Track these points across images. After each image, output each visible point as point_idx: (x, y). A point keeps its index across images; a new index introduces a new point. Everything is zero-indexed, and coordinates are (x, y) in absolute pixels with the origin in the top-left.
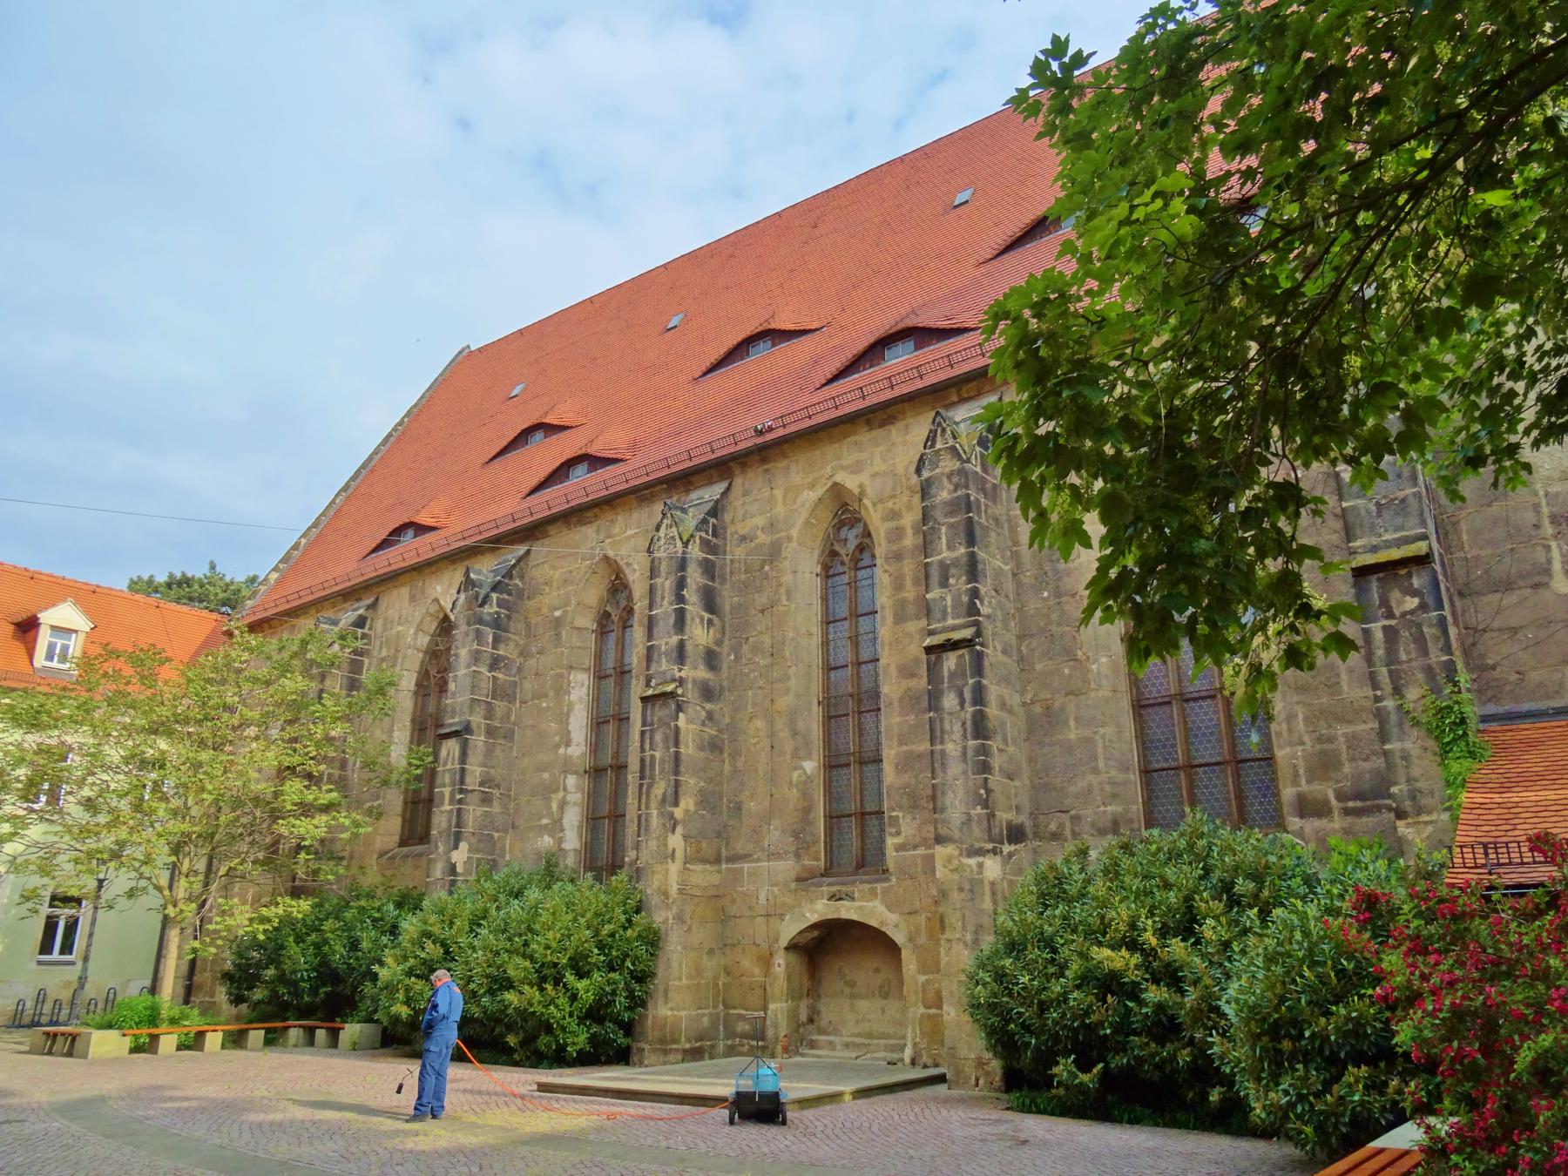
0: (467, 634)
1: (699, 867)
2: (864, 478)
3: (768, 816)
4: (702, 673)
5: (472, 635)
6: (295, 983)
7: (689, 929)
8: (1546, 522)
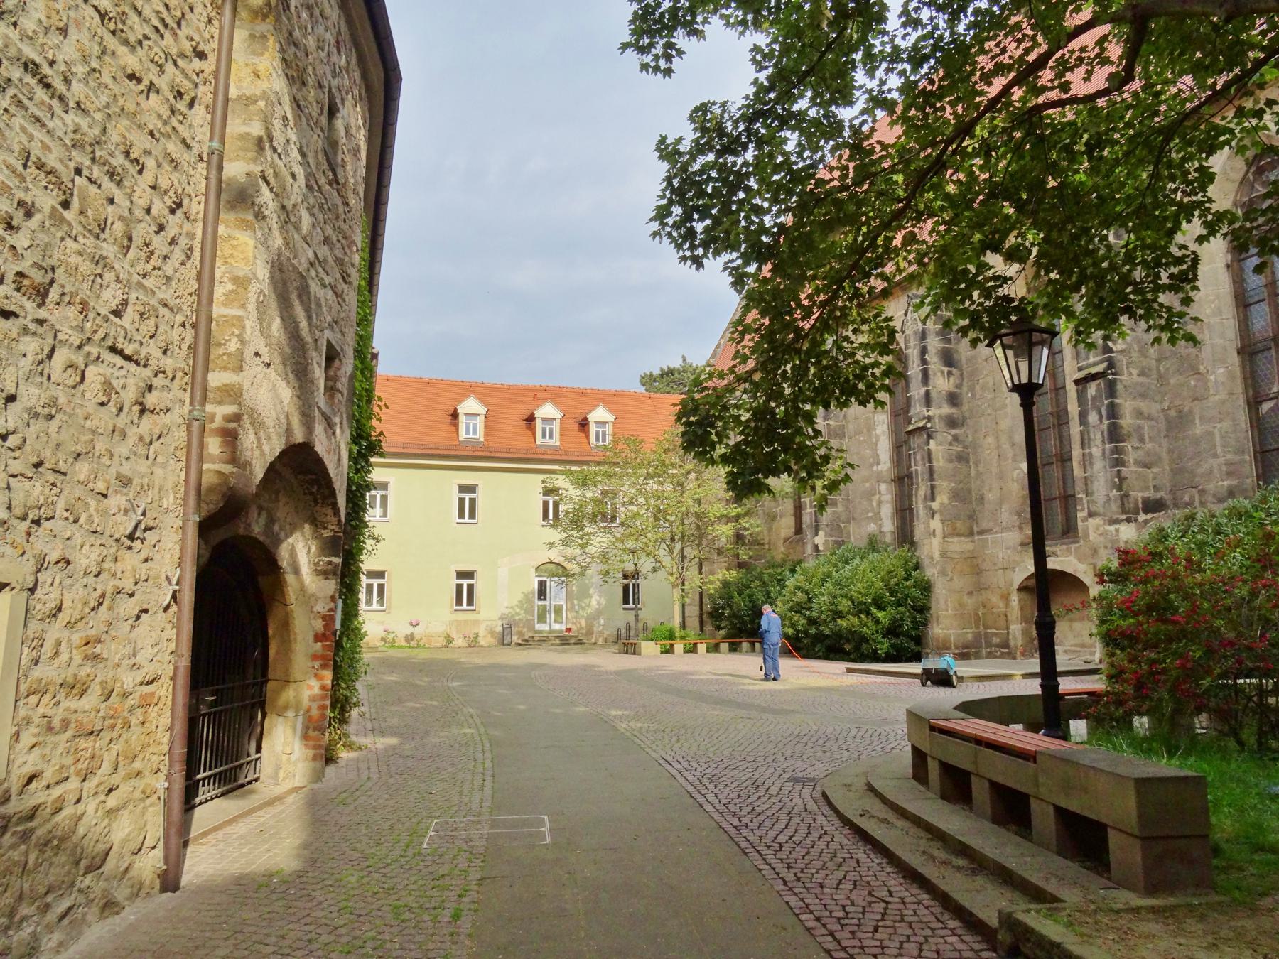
1: (956, 540)
3: (1001, 502)
4: (946, 410)
6: (741, 617)
7: (951, 579)
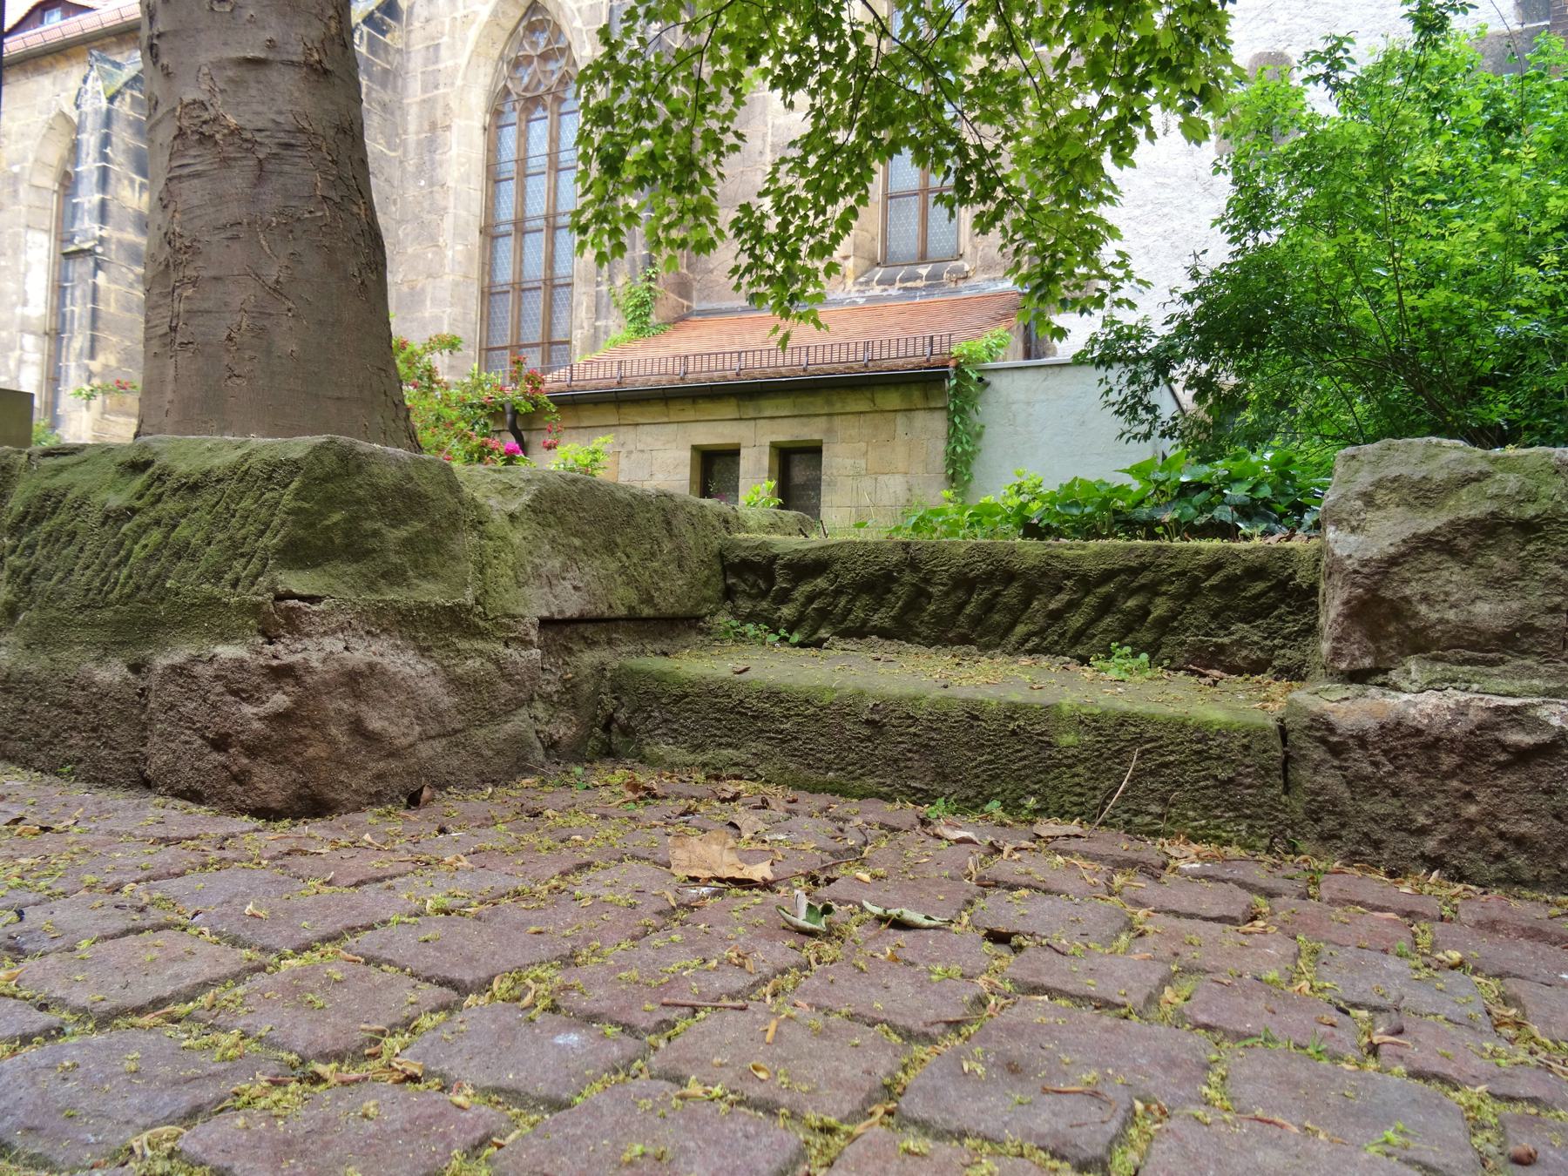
8: (768, 150)
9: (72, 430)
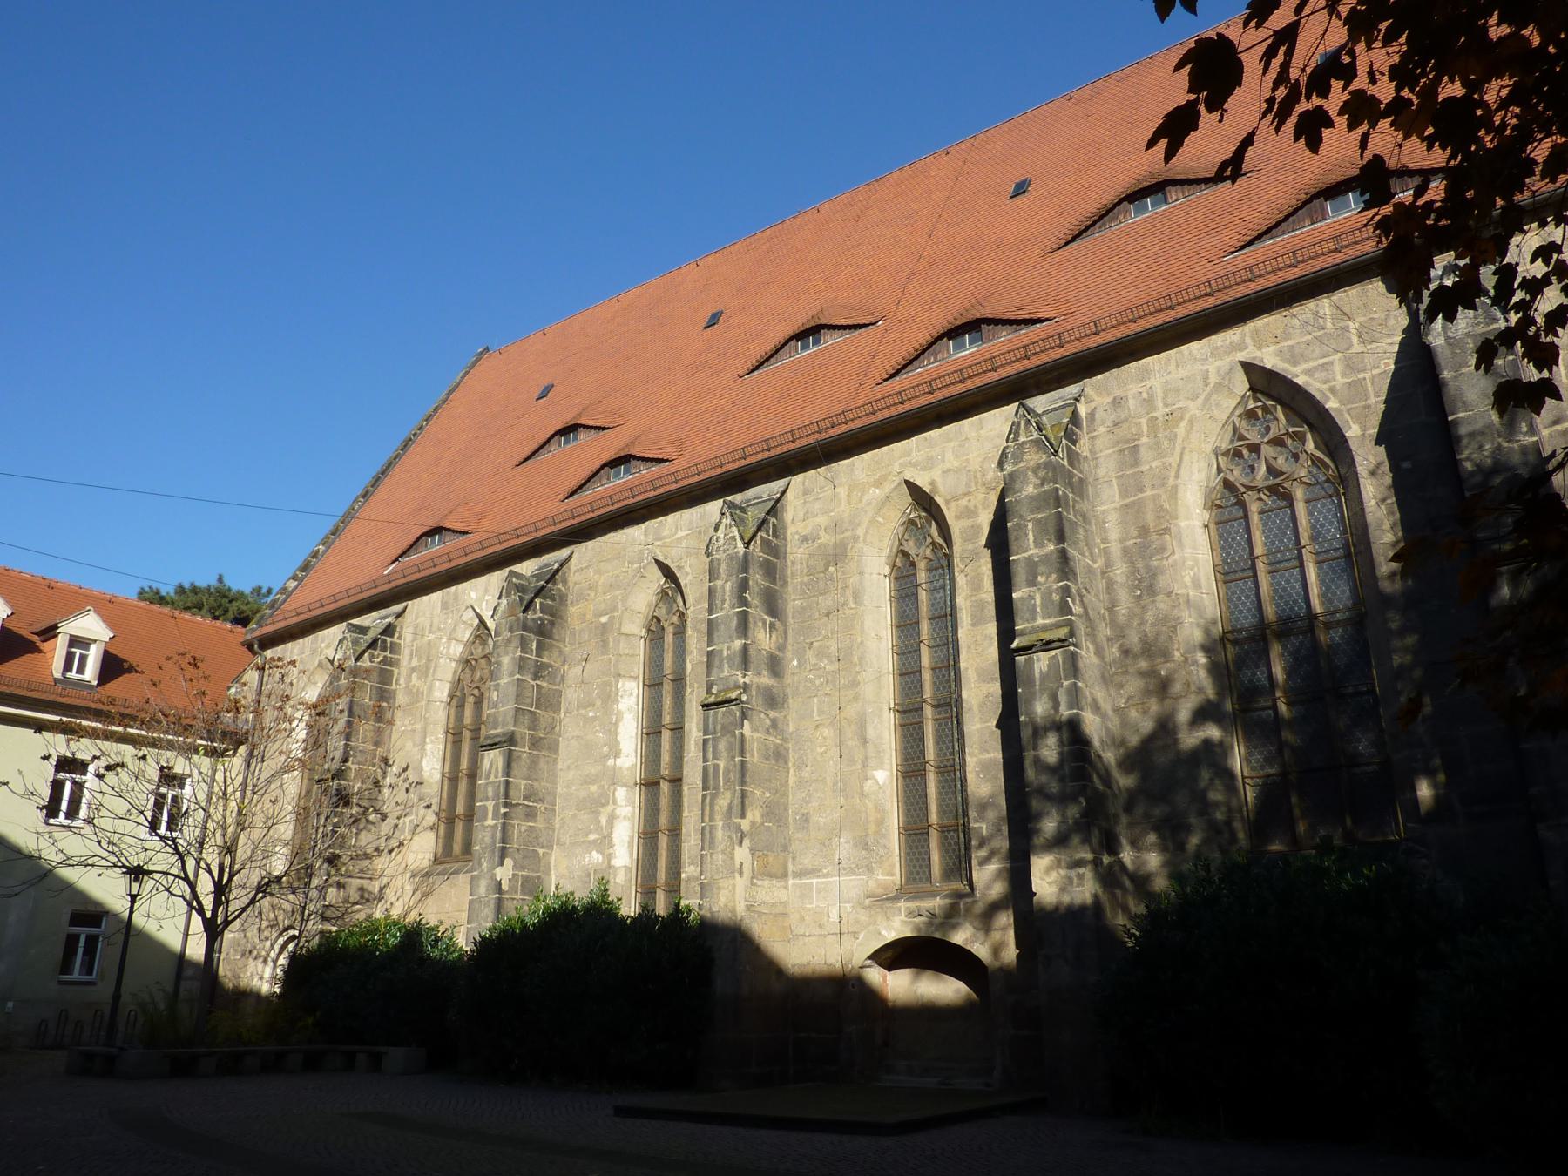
0: (509, 641)
2: (936, 474)
4: (766, 680)
5: (516, 642)
9: (722, 900)
